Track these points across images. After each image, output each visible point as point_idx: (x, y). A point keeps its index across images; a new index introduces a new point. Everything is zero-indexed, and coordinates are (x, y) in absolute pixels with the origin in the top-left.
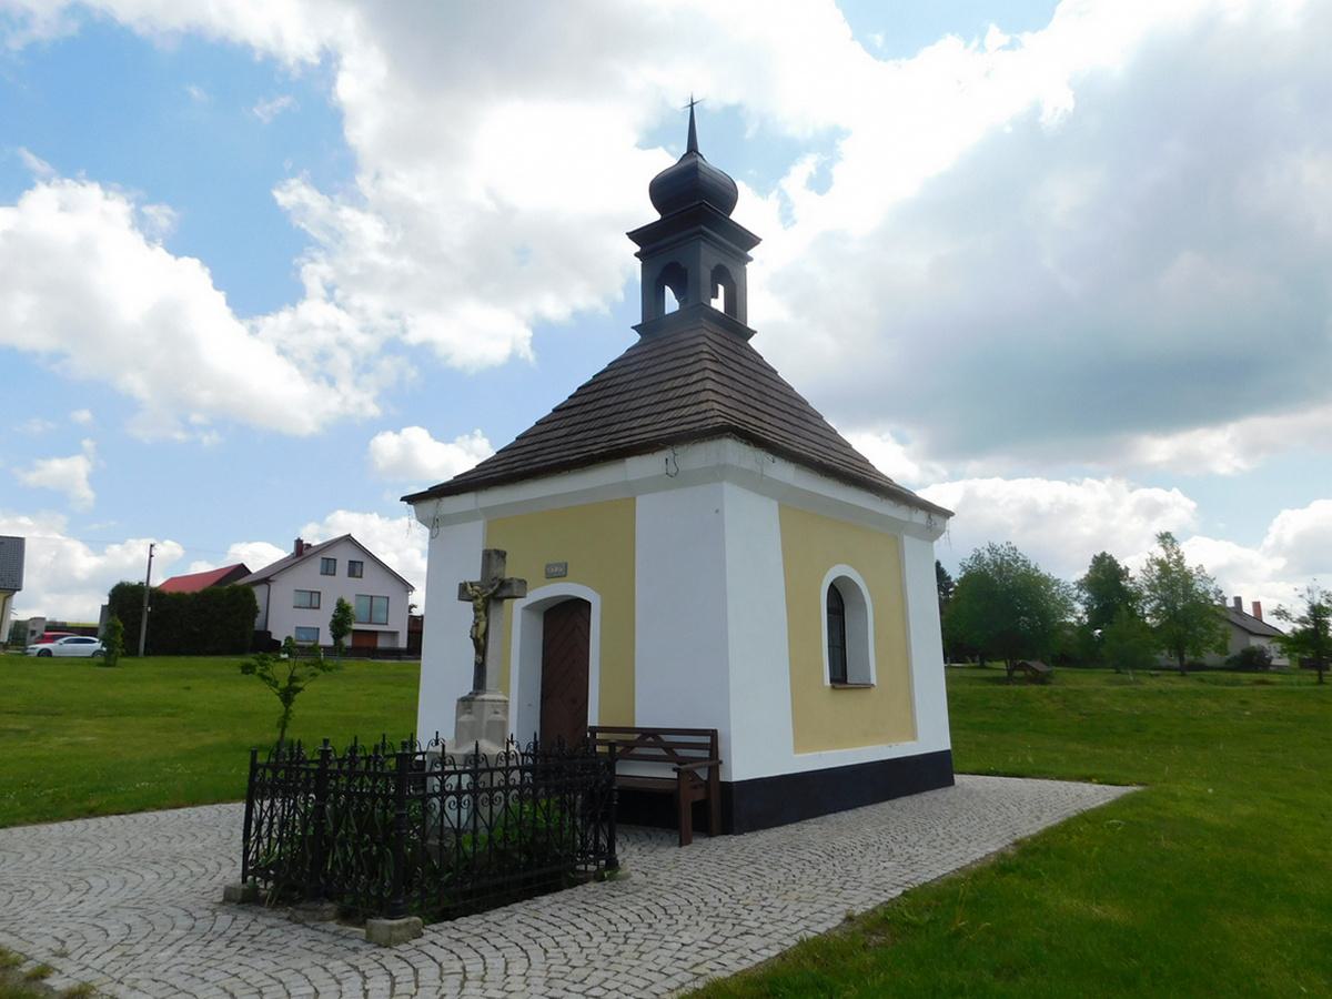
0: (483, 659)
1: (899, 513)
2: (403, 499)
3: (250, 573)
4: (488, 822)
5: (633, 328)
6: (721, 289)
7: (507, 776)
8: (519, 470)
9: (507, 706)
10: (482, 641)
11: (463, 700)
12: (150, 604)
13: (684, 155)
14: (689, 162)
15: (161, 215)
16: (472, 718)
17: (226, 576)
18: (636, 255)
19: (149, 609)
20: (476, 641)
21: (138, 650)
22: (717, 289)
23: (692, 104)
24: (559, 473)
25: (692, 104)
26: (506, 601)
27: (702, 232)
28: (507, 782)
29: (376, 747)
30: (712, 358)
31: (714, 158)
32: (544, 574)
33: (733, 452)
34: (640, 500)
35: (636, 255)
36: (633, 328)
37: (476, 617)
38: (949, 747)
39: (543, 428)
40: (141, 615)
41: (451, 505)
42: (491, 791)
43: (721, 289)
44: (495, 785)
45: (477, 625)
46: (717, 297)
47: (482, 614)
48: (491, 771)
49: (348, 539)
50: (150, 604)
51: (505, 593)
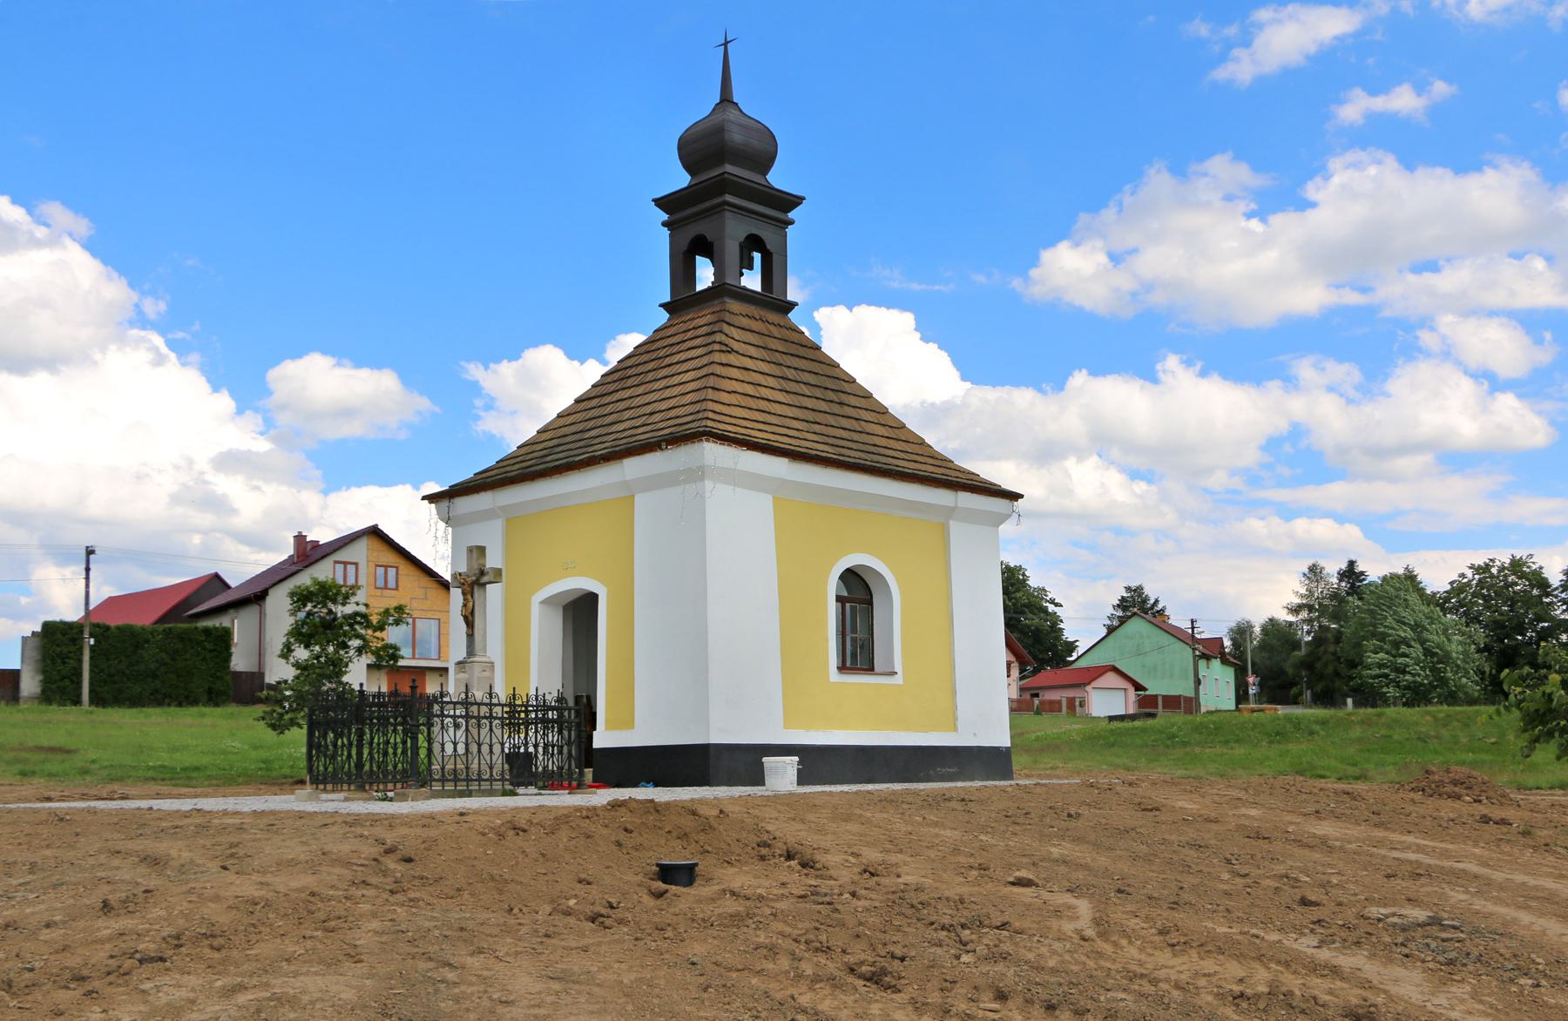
0: (472, 631)
1: (966, 499)
2: (424, 498)
3: (228, 587)
4: (489, 762)
5: (661, 306)
6: (757, 256)
7: (491, 710)
8: (531, 469)
9: (493, 666)
10: (470, 618)
11: (459, 663)
12: (91, 635)
13: (717, 105)
14: (719, 117)
15: (344, 488)
16: (466, 675)
17: (198, 590)
18: (664, 224)
19: (92, 641)
20: (466, 618)
21: (79, 695)
22: (751, 259)
23: (726, 44)
24: (560, 473)
25: (726, 44)
26: (488, 586)
27: (725, 209)
28: (491, 713)
29: (387, 612)
30: (724, 348)
31: (752, 103)
32: (1151, 592)
33: (711, 451)
34: (639, 499)
35: (664, 224)
36: (661, 306)
37: (465, 600)
38: (1008, 744)
39: (563, 421)
40: (81, 650)
41: (464, 504)
42: (479, 718)
43: (757, 256)
44: (482, 714)
45: (465, 605)
46: (751, 268)
47: (469, 597)
48: (479, 705)
49: (375, 533)
50: (91, 635)
51: (485, 579)
